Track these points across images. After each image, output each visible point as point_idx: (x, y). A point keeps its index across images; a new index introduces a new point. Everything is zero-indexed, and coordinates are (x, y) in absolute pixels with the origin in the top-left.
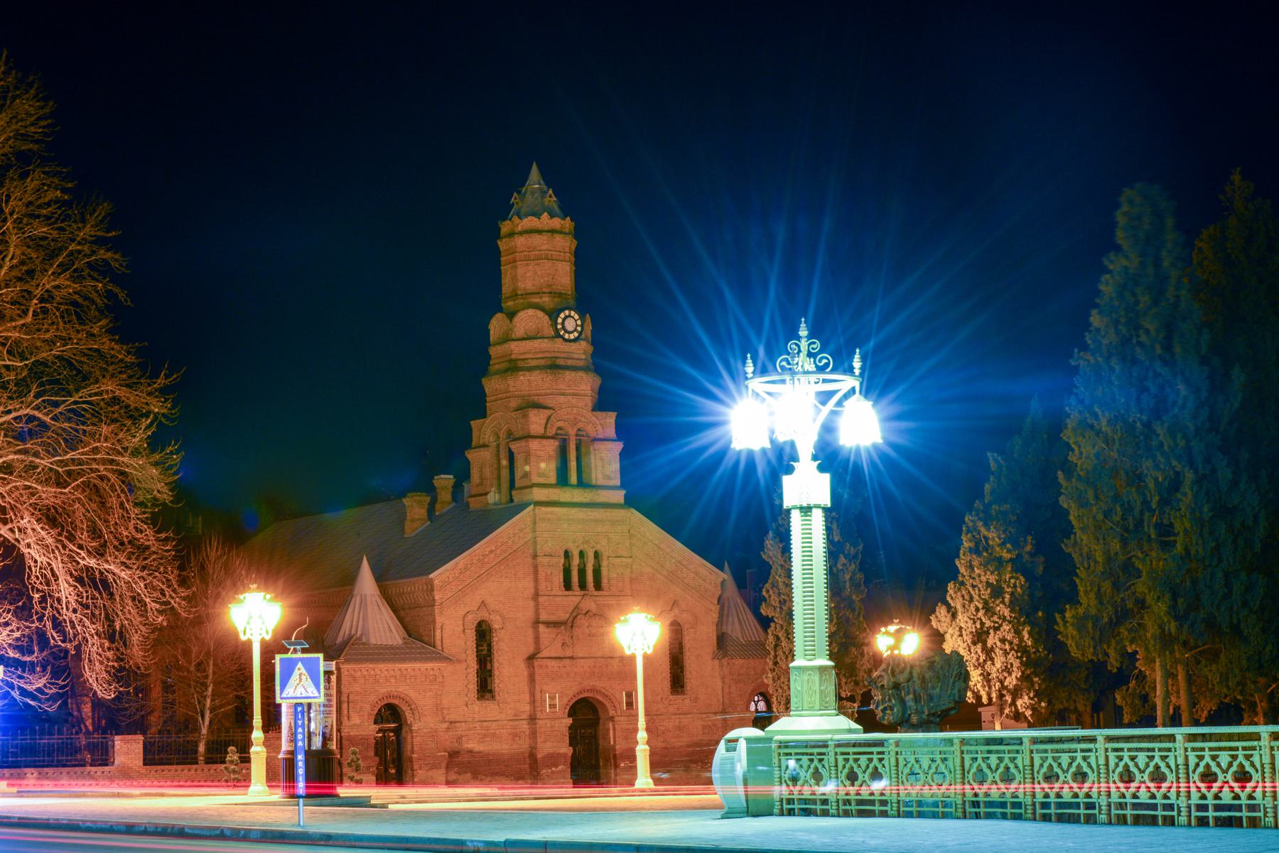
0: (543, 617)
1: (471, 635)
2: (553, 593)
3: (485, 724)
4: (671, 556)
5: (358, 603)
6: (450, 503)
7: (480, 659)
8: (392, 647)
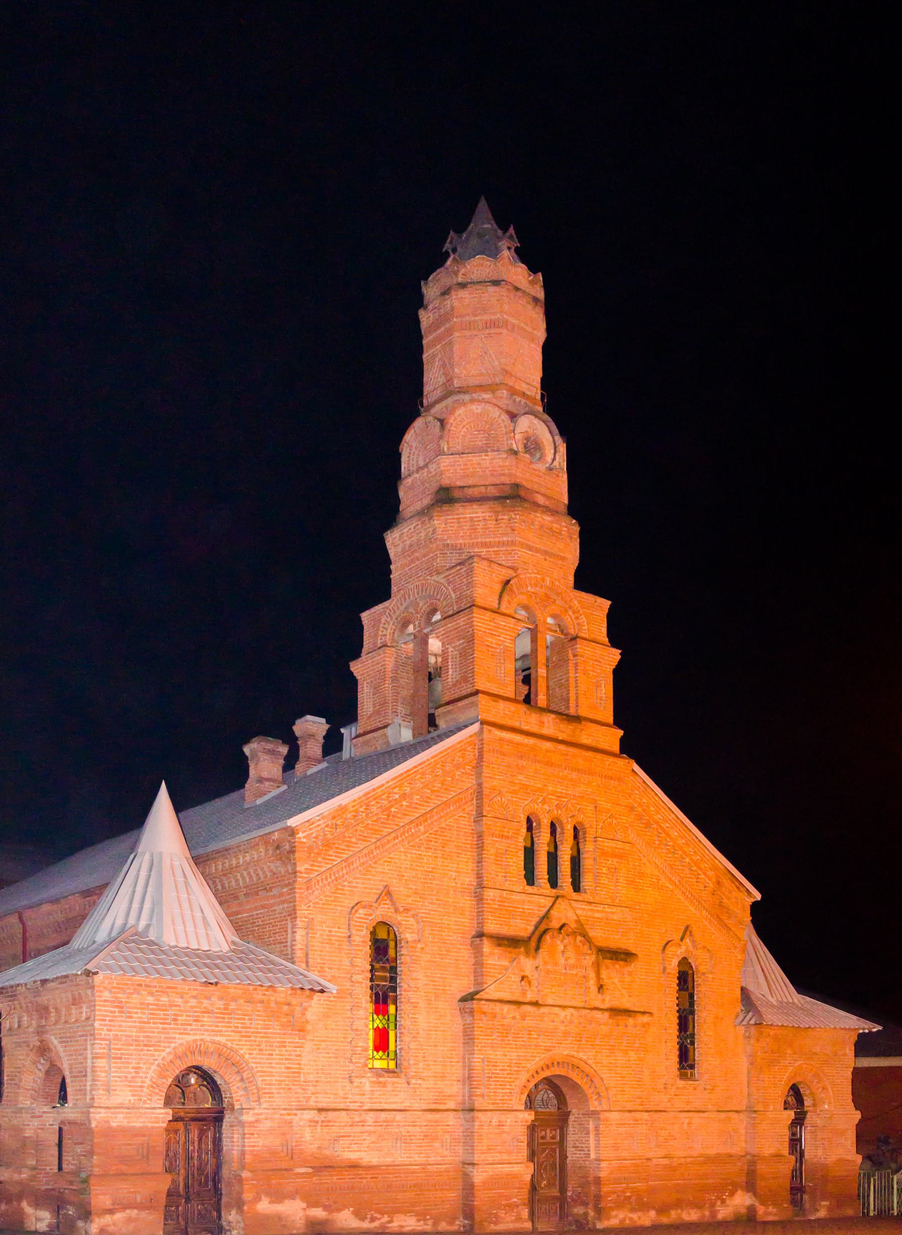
0: (491, 927)
1: (365, 950)
2: (507, 886)
3: (383, 1115)
4: (684, 852)
5: (143, 873)
6: (319, 762)
7: (377, 994)
8: (207, 955)
